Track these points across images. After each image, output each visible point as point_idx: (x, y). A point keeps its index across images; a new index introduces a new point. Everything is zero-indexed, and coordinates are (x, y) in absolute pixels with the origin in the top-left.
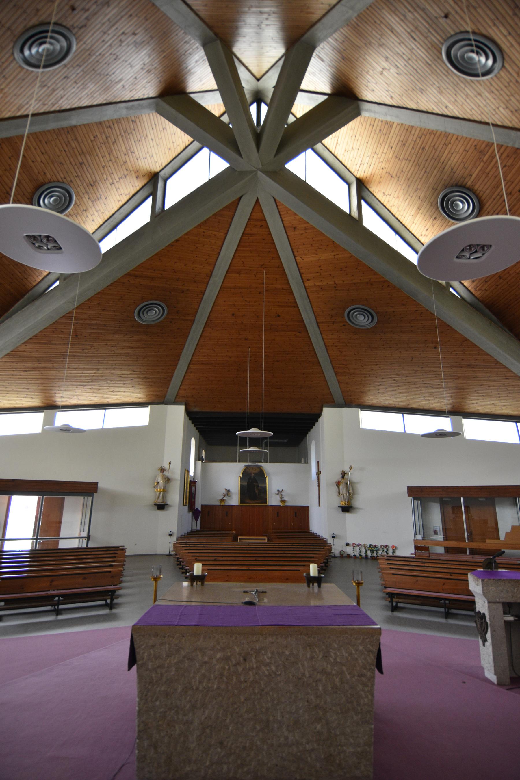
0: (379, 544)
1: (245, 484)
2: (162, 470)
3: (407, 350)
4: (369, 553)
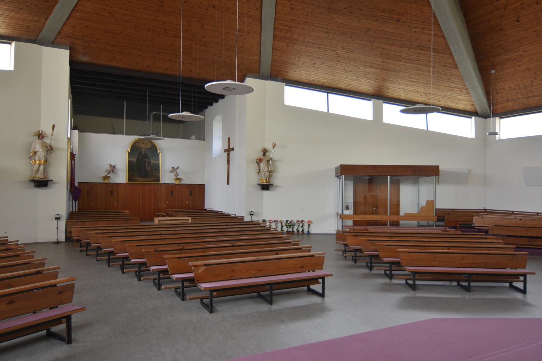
0: (295, 220)
1: (134, 160)
2: (40, 136)
3: (367, 19)
4: (285, 229)
